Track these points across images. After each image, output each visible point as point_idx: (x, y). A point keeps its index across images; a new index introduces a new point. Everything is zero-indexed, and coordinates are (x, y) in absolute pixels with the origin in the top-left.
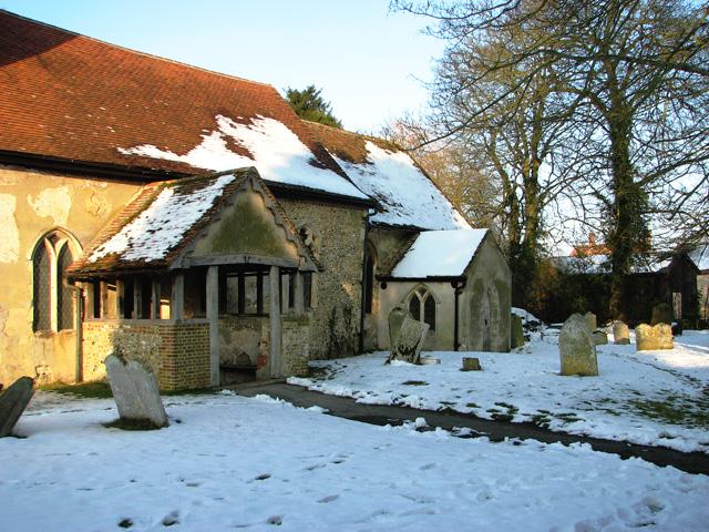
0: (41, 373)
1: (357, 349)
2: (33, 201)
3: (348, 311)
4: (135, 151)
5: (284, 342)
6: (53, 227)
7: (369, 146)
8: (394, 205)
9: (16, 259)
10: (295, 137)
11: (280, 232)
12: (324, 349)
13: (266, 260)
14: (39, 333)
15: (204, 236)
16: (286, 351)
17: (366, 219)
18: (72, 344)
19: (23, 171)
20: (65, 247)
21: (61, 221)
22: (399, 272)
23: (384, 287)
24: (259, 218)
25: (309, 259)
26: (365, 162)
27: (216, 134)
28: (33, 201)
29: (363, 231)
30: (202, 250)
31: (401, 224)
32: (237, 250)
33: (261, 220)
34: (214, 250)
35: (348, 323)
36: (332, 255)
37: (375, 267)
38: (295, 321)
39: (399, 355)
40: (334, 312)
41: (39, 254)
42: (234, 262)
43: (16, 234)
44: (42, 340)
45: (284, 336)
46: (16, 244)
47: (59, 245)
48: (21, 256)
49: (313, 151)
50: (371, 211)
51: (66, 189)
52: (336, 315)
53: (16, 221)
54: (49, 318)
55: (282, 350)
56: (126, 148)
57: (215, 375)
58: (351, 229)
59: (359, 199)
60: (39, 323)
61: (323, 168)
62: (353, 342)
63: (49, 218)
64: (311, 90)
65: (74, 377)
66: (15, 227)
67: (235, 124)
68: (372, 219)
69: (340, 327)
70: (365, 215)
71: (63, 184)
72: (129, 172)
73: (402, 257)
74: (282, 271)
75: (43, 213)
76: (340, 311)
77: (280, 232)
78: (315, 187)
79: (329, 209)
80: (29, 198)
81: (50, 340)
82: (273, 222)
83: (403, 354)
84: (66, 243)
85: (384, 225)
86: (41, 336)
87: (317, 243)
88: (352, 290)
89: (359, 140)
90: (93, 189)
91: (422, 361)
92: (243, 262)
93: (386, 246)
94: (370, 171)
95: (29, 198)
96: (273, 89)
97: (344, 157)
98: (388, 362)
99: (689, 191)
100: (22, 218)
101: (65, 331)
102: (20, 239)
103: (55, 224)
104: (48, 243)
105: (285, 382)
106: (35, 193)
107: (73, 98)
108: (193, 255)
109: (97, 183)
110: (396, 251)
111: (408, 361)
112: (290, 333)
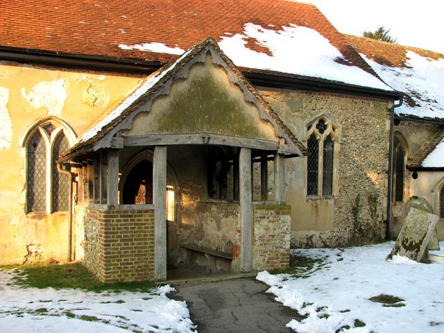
0: (34, 251)
1: (383, 236)
2: (27, 93)
3: (373, 200)
4: (137, 47)
5: (257, 231)
6: (47, 117)
7: (409, 54)
8: (428, 100)
9: (8, 146)
10: (327, 41)
11: (251, 111)
12: (347, 236)
13: (232, 141)
14: (32, 214)
15: (147, 113)
16: (258, 242)
17: (391, 110)
18: (65, 225)
19: (16, 65)
20: (61, 135)
21: (55, 111)
22: (428, 163)
23: (415, 176)
24: (225, 95)
25: (289, 140)
26: (403, 65)
27: (238, 37)
28: (27, 93)
29: (388, 123)
30: (142, 130)
31: (433, 117)
32: (193, 129)
33: (226, 98)
34: (161, 129)
35: (373, 212)
36: (354, 145)
37: (406, 158)
38: (272, 208)
39: (402, 248)
40: (358, 200)
41: (32, 142)
42: (189, 142)
43: (9, 124)
44: (34, 221)
45: (257, 225)
46: (9, 133)
47: (54, 134)
48: (13, 144)
49: (342, 52)
50: (397, 102)
51: (61, 81)
52: (360, 203)
53: (9, 112)
54: (44, 201)
55: (254, 241)
56: (129, 45)
57: (161, 267)
58: (375, 120)
59: (383, 91)
60: (31, 204)
61: (349, 65)
62: (380, 229)
63: (44, 108)
64: (381, 30)
65: (66, 257)
66: (8, 117)
67: (263, 29)
68: (398, 111)
69: (364, 214)
70: (390, 106)
71: (59, 77)
72: (122, 63)
73: (433, 148)
74: (255, 152)
75: (37, 104)
76: (364, 199)
77: (251, 111)
78: (332, 79)
79: (351, 100)
80: (23, 90)
81: (42, 222)
82: (242, 100)
83: (407, 249)
84: (62, 131)
85: (413, 118)
86: (34, 217)
87: (338, 133)
88: (378, 179)
89: (401, 51)
90: (90, 81)
91: (431, 258)
92: (200, 142)
93: (416, 138)
94: (408, 73)
95: (23, 90)
96: (314, 7)
97: (380, 61)
98: (390, 257)
99: (417, 241)
100: (14, 108)
101: (59, 213)
102: (13, 127)
103: (50, 114)
104: (42, 131)
105: (253, 278)
106: (29, 86)
107: (98, 9)
108: (130, 134)
109: (94, 76)
110: (428, 143)
111: (414, 258)
112: (265, 222)
